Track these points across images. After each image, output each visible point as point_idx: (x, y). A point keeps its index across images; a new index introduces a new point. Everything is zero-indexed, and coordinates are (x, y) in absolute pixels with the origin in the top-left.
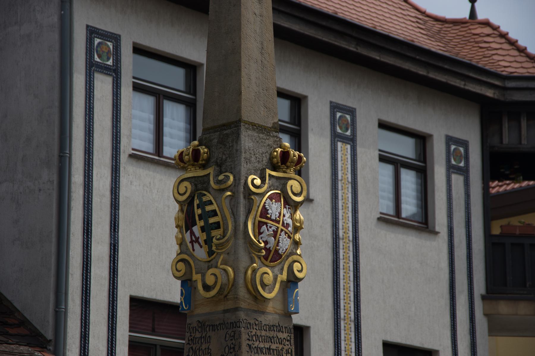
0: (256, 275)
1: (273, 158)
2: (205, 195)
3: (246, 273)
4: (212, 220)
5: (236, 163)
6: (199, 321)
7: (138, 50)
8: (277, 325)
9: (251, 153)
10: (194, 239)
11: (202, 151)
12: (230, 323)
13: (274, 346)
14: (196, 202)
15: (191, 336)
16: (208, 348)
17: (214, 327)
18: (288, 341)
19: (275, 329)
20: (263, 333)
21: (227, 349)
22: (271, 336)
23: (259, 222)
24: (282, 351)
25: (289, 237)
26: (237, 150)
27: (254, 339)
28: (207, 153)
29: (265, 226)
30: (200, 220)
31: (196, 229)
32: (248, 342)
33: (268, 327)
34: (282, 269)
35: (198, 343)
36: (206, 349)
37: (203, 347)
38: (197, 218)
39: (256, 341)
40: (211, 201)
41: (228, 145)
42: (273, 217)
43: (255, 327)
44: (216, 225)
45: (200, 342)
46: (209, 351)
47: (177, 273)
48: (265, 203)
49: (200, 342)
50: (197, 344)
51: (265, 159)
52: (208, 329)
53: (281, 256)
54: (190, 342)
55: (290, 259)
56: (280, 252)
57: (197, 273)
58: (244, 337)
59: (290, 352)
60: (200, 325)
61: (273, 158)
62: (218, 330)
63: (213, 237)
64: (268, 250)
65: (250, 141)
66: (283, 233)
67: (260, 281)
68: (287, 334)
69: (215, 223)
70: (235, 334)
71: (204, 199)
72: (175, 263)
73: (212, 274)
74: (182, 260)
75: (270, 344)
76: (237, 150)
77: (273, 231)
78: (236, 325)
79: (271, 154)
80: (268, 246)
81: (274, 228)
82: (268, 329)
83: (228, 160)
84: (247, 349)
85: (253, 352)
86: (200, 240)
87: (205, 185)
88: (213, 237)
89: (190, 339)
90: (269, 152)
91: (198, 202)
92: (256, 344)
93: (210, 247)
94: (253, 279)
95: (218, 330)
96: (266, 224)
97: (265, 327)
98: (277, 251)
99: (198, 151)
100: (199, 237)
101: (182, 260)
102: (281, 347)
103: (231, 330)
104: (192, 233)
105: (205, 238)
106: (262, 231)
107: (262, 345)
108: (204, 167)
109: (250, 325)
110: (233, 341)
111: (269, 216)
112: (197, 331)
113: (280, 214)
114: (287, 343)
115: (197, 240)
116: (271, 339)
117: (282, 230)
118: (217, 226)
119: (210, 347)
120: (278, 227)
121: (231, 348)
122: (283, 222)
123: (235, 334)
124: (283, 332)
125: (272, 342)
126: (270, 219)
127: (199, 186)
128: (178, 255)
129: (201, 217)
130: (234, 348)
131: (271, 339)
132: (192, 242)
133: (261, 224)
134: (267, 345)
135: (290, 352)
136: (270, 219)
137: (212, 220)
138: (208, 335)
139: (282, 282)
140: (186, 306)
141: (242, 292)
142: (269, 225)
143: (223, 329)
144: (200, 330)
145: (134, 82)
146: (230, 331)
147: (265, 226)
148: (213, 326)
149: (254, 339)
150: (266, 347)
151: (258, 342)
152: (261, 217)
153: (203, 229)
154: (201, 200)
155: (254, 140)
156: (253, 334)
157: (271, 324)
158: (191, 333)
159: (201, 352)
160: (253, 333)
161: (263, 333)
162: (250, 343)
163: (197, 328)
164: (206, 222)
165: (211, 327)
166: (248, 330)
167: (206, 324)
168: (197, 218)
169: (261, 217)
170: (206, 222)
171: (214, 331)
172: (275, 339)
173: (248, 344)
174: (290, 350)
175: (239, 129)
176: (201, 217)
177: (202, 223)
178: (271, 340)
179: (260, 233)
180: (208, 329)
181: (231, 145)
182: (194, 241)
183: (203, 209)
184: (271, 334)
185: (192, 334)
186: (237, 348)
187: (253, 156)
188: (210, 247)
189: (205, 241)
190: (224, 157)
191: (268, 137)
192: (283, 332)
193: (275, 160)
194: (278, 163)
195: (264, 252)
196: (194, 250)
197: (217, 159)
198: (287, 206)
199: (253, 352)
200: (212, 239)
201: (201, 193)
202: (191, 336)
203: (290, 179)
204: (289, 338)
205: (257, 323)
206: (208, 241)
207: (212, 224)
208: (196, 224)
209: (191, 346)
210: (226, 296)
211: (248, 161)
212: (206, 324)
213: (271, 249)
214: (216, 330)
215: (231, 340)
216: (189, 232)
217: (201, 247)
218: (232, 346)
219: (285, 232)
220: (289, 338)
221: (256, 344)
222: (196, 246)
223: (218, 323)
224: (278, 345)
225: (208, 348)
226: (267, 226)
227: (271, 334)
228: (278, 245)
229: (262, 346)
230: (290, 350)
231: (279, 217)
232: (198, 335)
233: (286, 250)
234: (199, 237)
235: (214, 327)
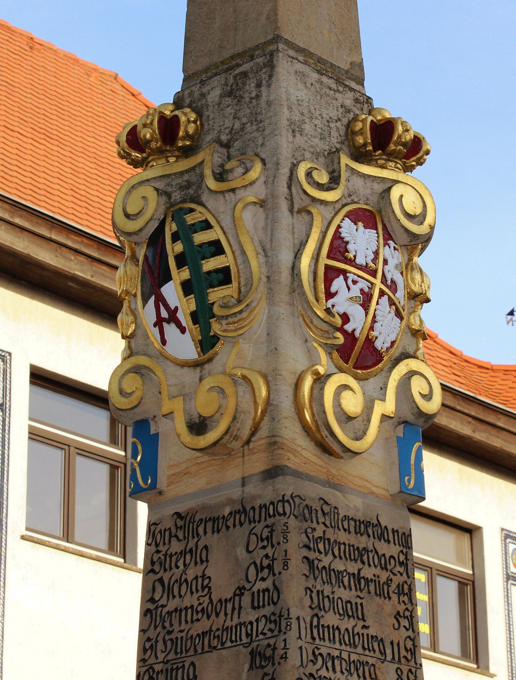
0: (322, 389)
1: (354, 133)
2: (192, 210)
3: (297, 386)
4: (210, 265)
5: (266, 132)
6: (178, 515)
7: (40, 378)
8: (376, 522)
9: (302, 114)
10: (164, 314)
11: (183, 119)
12: (260, 507)
13: (368, 572)
14: (171, 228)
15: (158, 552)
16: (203, 576)
17: (217, 523)
18: (401, 564)
19: (370, 532)
20: (342, 537)
21: (252, 571)
22: (361, 547)
23: (327, 267)
24: (389, 586)
25: (399, 314)
26: (269, 104)
27: (321, 546)
28: (195, 122)
29: (342, 277)
30: (179, 266)
31: (171, 292)
32: (305, 552)
33: (352, 523)
34: (384, 388)
35: (177, 567)
36: (196, 578)
37: (191, 574)
38: (172, 263)
39: (326, 554)
40: (206, 221)
41: (246, 95)
42: (360, 260)
43: (321, 520)
44: (221, 276)
45: (181, 563)
46: (206, 582)
47: (124, 400)
48: (339, 227)
49: (181, 563)
50: (174, 570)
51: (334, 134)
52: (201, 530)
53: (378, 356)
54: (157, 568)
55: (402, 369)
56: (378, 344)
57: (172, 397)
58: (295, 539)
59: (406, 591)
60: (180, 523)
61: (354, 133)
62: (228, 527)
63: (213, 304)
64: (351, 337)
65: (301, 86)
66: (385, 298)
67: (334, 407)
68: (398, 549)
69: (217, 271)
70: (271, 532)
71: (190, 219)
72: (117, 380)
73: (211, 389)
74: (137, 370)
75: (360, 565)
76: (269, 104)
77: (362, 291)
78: (275, 509)
79: (349, 126)
80: (349, 327)
81: (363, 284)
82: (352, 529)
83: (249, 128)
84: (305, 568)
85: (319, 580)
86: (180, 315)
87: (191, 191)
88: (213, 304)
89: (155, 559)
90: (345, 121)
91: (174, 227)
92: (326, 560)
93: (206, 329)
94: (317, 396)
95: (228, 527)
96: (344, 272)
97: (346, 524)
98: (369, 342)
99: (175, 119)
100: (176, 308)
101: (137, 370)
102: (384, 576)
103: (263, 524)
104: (160, 300)
105: (193, 307)
106: (333, 289)
107: (339, 565)
108: (187, 152)
109: (310, 513)
110: (269, 551)
111: (351, 255)
112: (173, 539)
113: (376, 253)
114: (398, 568)
115: (173, 317)
116: (360, 554)
117: (382, 293)
118: (224, 276)
119: (208, 573)
120: (372, 284)
121: (262, 568)
122: (384, 275)
123: (271, 532)
124: (389, 542)
125: (363, 563)
126: (352, 262)
127: (177, 196)
128: (124, 359)
129: (181, 261)
130: (270, 567)
131: (360, 554)
132: (159, 323)
133: (331, 274)
134: (353, 567)
135: (406, 591)
136: (352, 262)
137: (210, 265)
138: (201, 545)
139: (385, 418)
140: (145, 481)
141: (291, 433)
142: (351, 277)
143: (241, 524)
144: (180, 535)
145: (30, 427)
146: (259, 528)
147: (342, 277)
148: (214, 520)
149: (321, 546)
150: (351, 570)
151: (330, 557)
152: (329, 257)
153: (187, 288)
154: (181, 223)
155: (309, 85)
156: (317, 534)
157: (360, 516)
158: (157, 545)
159: (184, 585)
160: (319, 533)
161: (342, 537)
162: (312, 555)
163: (173, 530)
164: (196, 270)
165: (210, 525)
166: (305, 525)
167: (197, 518)
168: (172, 263)
169: (329, 257)
170: (196, 270)
171: (219, 531)
172: (371, 555)
173: (306, 557)
174: (406, 587)
175: (271, 65)
176: (181, 261)
177: (186, 274)
178: (361, 556)
179: (330, 295)
180: (201, 530)
181: (254, 94)
182: (164, 320)
183: (188, 242)
184: (363, 542)
185: (161, 548)
186: (278, 567)
187: (307, 120)
188: (206, 329)
189: (194, 316)
190: (237, 125)
191: (341, 89)
192: (389, 542)
193: (360, 140)
194: (365, 145)
195: (340, 339)
196: (164, 342)
197: (220, 131)
198: (391, 242)
199: (319, 580)
200: (211, 309)
201: (181, 209)
202: (158, 552)
203: (396, 182)
204: (402, 558)
205: (326, 509)
206: (202, 316)
207: (209, 273)
208: (168, 278)
209: (158, 576)
210: (248, 442)
211: (296, 129)
212: (197, 518)
213: (357, 334)
214: (224, 529)
215: (264, 547)
216: (153, 298)
217: (183, 330)
218: (266, 562)
219: (390, 298)
220: (402, 558)
221: (326, 560)
222: (170, 329)
223: (227, 511)
224: (378, 571)
225: (203, 576)
226: (346, 279)
227: (363, 542)
228: (372, 328)
229: (341, 568)
230: (406, 587)
231: (375, 260)
232: (176, 547)
233: (393, 343)
234: (176, 308)
235: (217, 523)
